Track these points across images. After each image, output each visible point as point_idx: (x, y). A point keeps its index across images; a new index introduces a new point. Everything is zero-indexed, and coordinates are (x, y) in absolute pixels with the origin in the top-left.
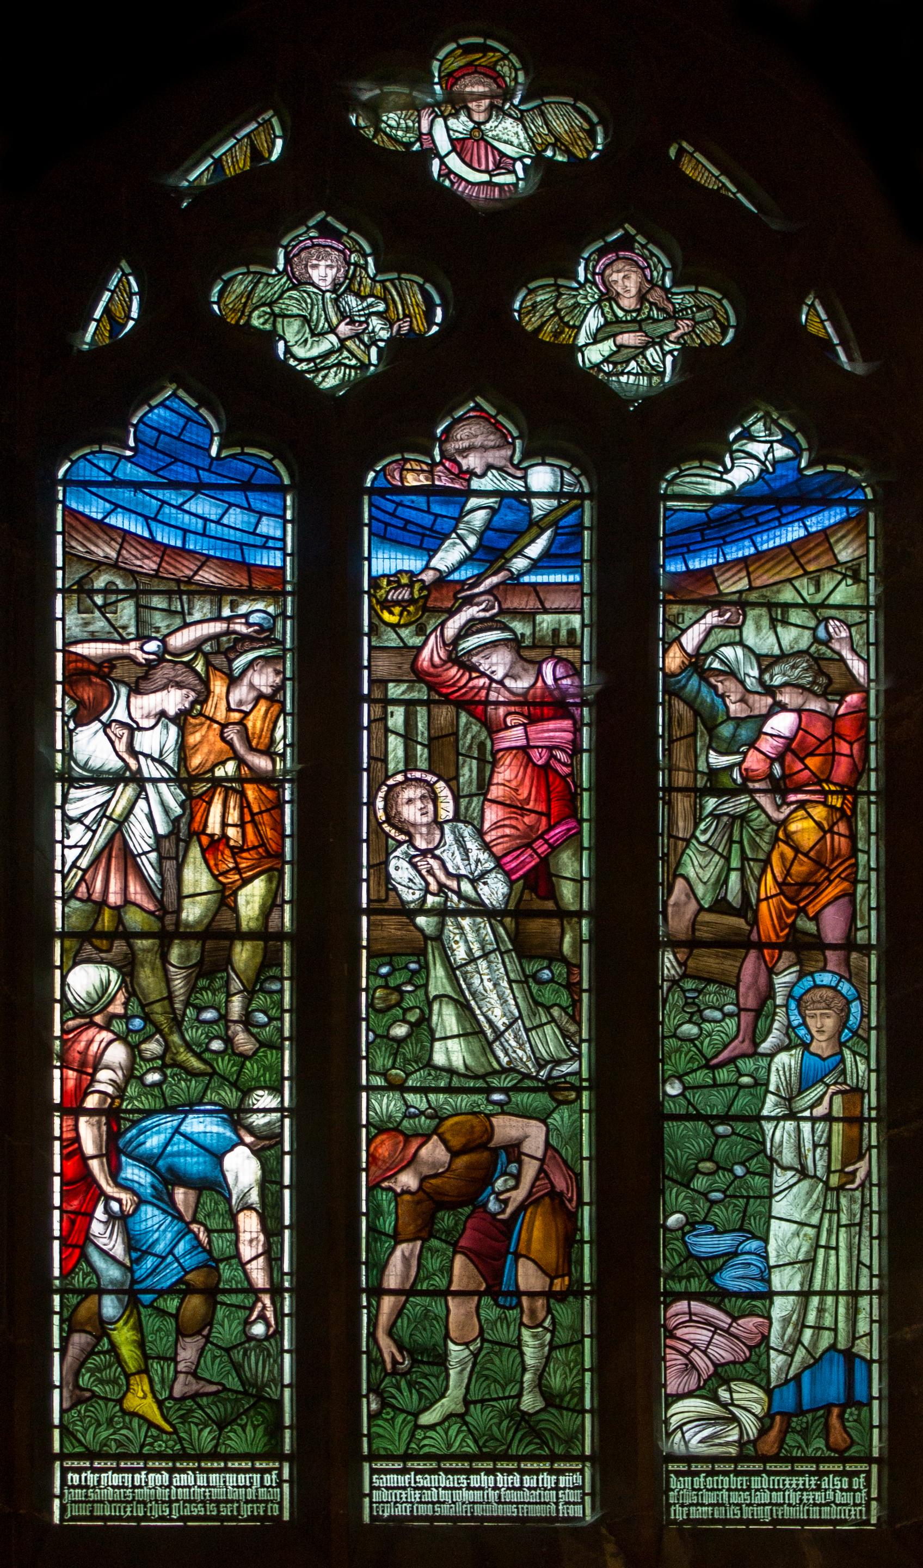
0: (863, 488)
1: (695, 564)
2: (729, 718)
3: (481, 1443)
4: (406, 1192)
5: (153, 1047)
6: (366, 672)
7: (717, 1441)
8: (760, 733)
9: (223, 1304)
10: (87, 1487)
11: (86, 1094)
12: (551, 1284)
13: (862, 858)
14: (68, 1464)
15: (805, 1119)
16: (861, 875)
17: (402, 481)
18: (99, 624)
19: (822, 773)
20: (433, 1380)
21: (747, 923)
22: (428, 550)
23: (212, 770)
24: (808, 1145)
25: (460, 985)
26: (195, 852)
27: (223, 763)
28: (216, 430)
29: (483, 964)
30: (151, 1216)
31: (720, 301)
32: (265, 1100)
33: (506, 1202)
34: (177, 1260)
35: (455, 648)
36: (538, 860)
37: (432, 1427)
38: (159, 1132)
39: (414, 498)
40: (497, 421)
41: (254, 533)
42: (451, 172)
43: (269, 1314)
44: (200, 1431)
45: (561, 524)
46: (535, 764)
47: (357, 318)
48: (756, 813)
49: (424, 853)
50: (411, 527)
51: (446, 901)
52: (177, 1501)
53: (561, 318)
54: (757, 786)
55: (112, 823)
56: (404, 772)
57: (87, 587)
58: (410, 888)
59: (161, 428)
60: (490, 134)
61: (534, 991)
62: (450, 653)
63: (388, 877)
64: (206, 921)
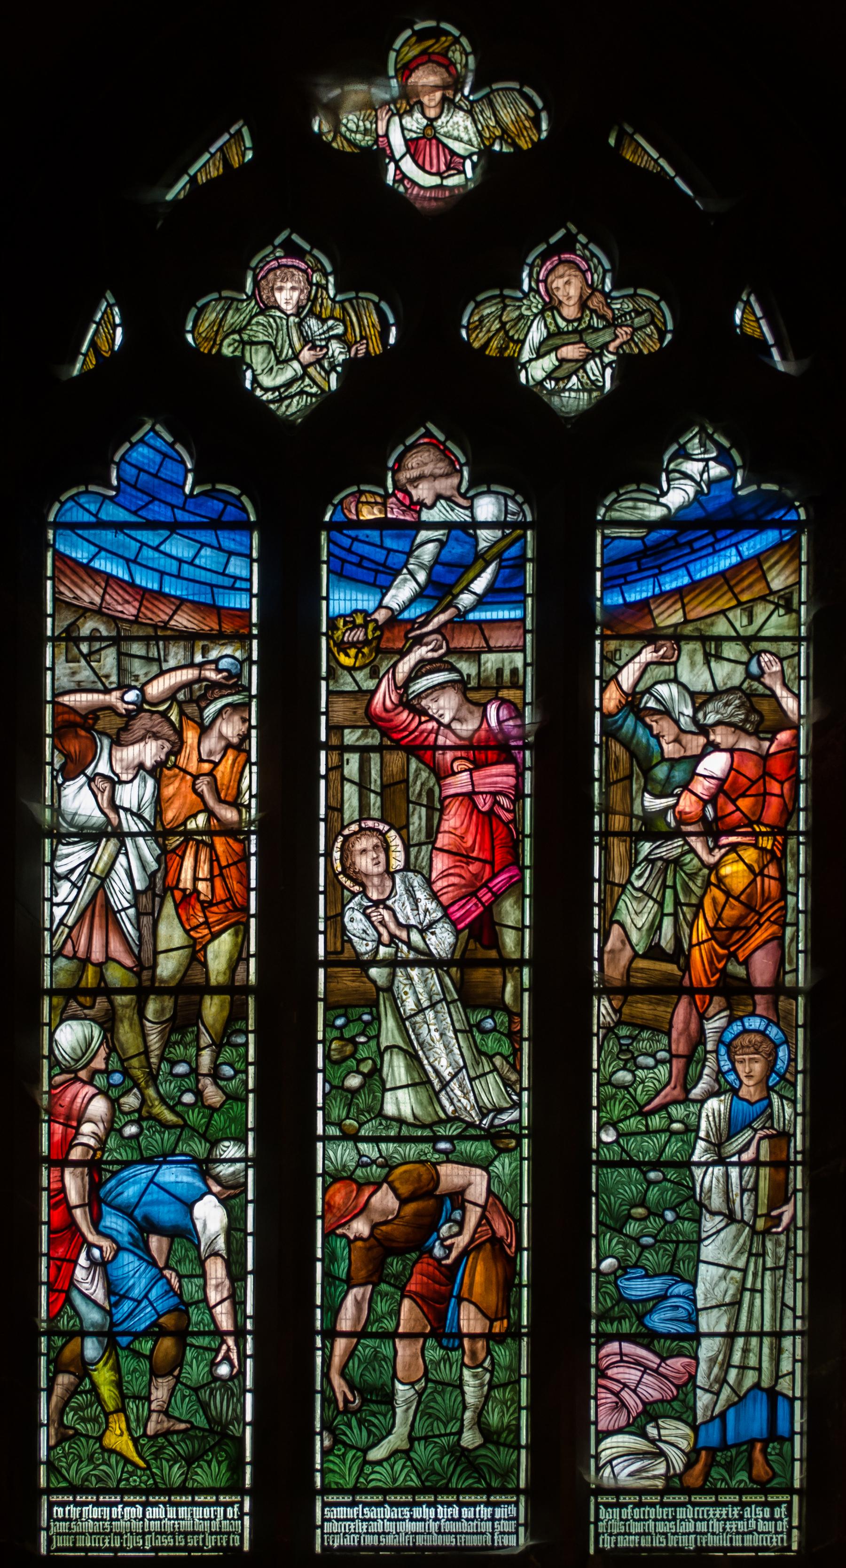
0: (797, 508)
1: (633, 596)
2: (663, 759)
3: (423, 1478)
4: (358, 1238)
5: (131, 1101)
6: (323, 719)
7: (645, 1475)
8: (694, 774)
9: (192, 1345)
10: (70, 1520)
11: (71, 1147)
12: (491, 1327)
13: (791, 900)
14: (54, 1498)
15: (733, 1164)
16: (790, 918)
17: (357, 515)
18: (85, 674)
19: (754, 814)
20: (381, 1418)
21: (680, 969)
22: (381, 587)
23: (184, 823)
24: (736, 1190)
25: (407, 1031)
26: (169, 908)
27: (195, 816)
28: (189, 466)
29: (430, 1014)
30: (129, 1262)
31: (657, 303)
32: (231, 1150)
33: (450, 1248)
34: (151, 1303)
35: (406, 691)
36: (481, 909)
37: (379, 1463)
38: (134, 1183)
39: (368, 532)
40: (447, 448)
41: (223, 574)
42: (405, 176)
43: (234, 1356)
44: (171, 1467)
45: (506, 555)
46: (479, 811)
47: (318, 343)
48: (688, 858)
49: (377, 904)
50: (366, 563)
51: (396, 952)
52: (150, 1533)
53: (507, 333)
54: (690, 828)
55: (95, 879)
56: (359, 821)
57: (75, 634)
58: (363, 939)
59: (140, 465)
60: (442, 131)
61: (478, 1041)
62: (401, 696)
63: (344, 928)
64: (179, 976)
